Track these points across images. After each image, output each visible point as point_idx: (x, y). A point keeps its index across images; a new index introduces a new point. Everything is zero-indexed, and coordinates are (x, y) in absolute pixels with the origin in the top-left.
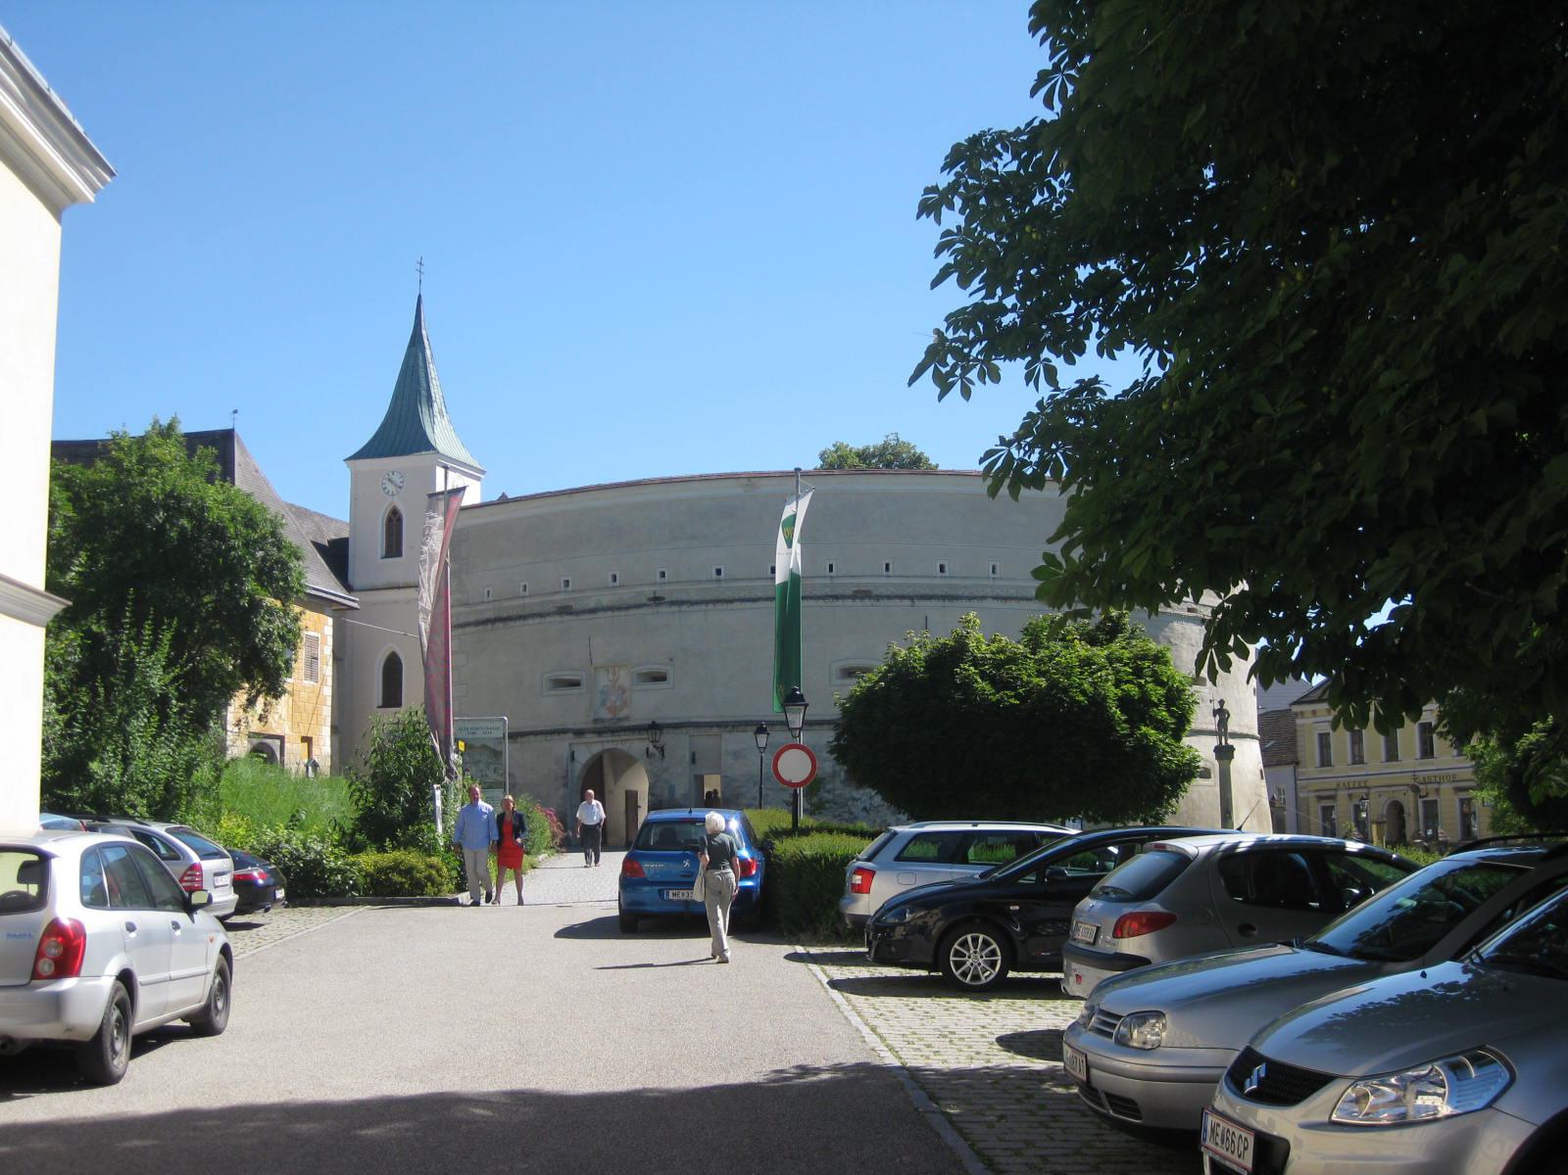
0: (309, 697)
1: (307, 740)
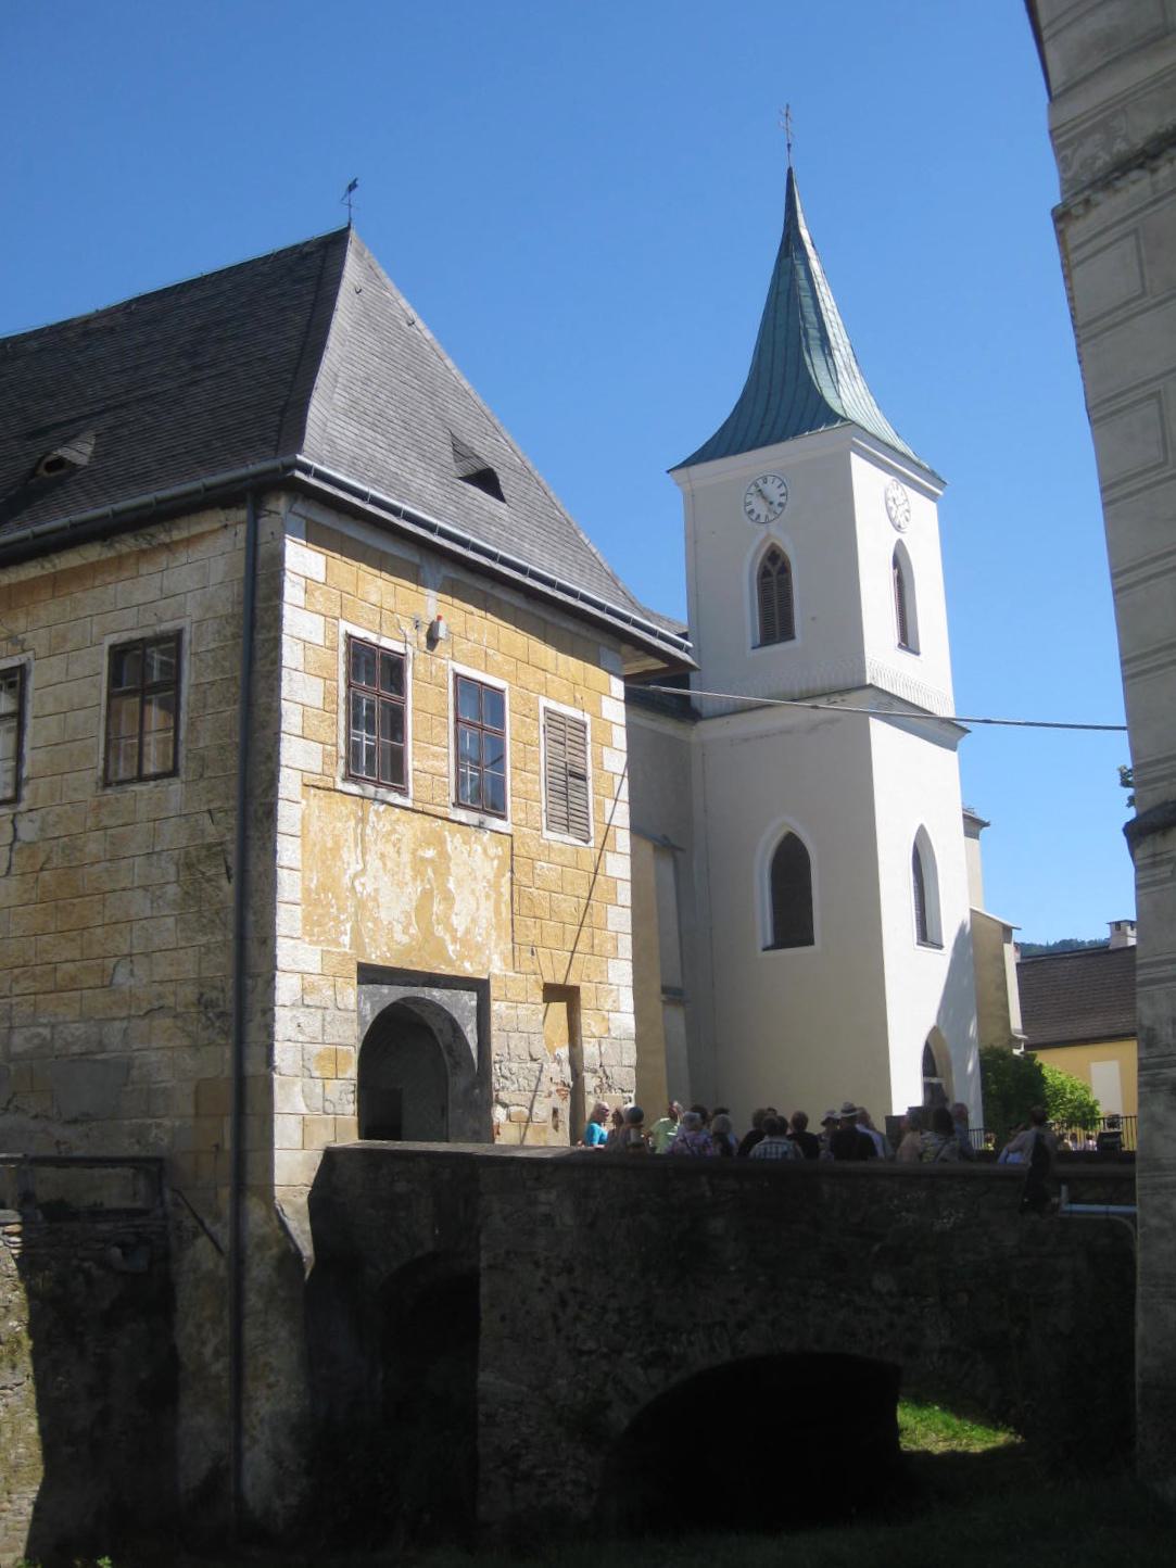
0: (562, 877)
1: (563, 994)
